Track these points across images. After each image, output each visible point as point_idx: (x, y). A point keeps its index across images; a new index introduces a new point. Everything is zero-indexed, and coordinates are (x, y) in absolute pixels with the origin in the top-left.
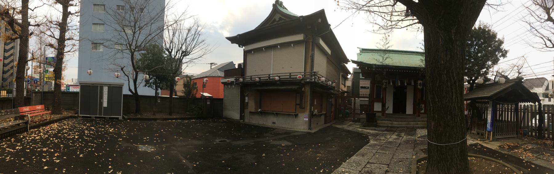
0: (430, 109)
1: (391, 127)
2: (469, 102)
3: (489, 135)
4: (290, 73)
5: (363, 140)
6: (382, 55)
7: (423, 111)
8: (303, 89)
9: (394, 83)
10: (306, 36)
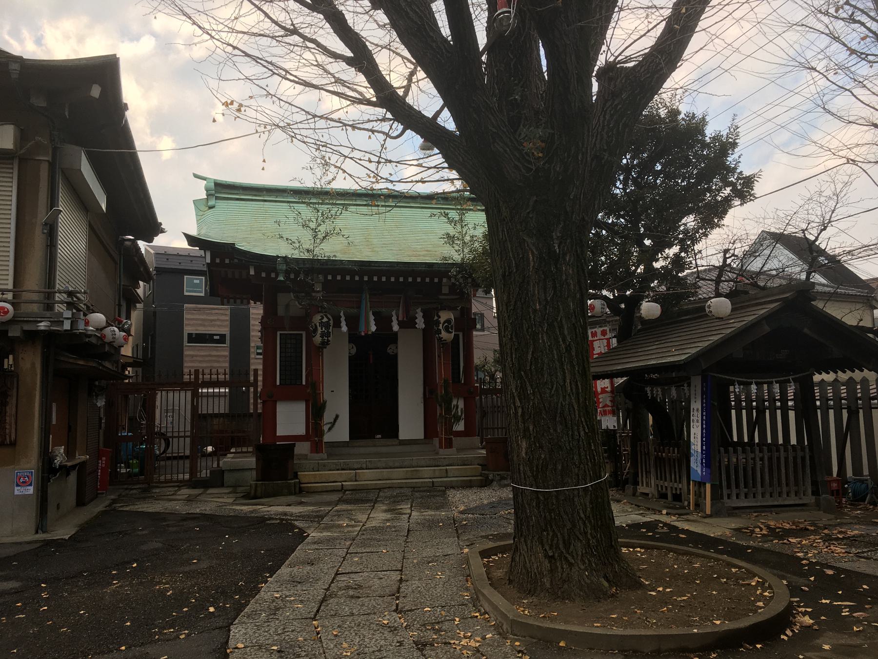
0: (516, 413)
1: (354, 490)
2: (620, 381)
3: (700, 495)
5: (284, 539)
6: (306, 212)
7: (460, 427)
9: (353, 322)
10: (22, 137)
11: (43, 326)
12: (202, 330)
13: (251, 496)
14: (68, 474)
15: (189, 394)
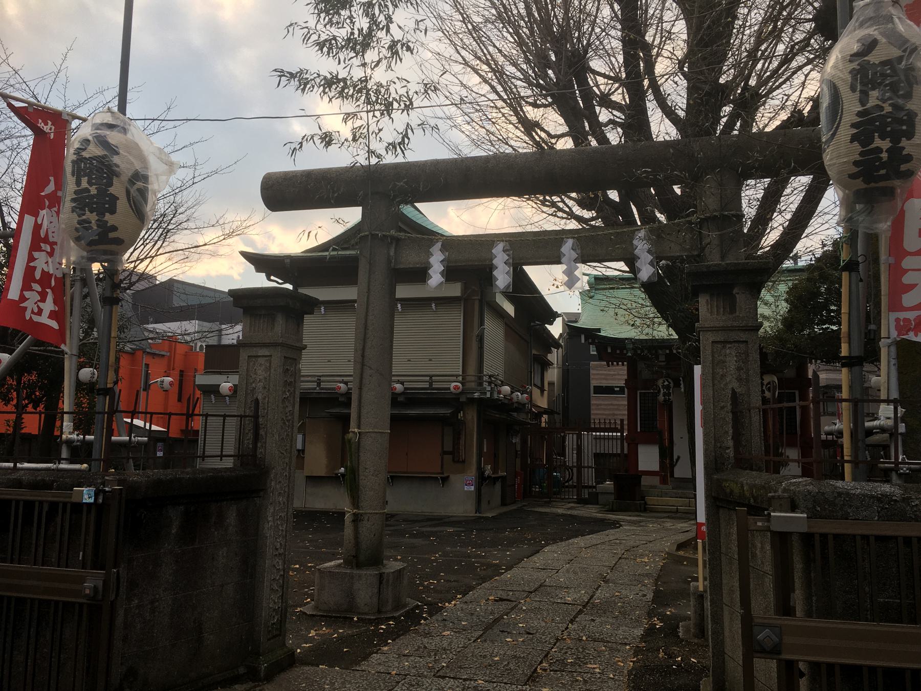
4: (431, 377)
8: (461, 415)
10: (465, 289)
11: (476, 395)
12: (604, 383)
13: (612, 511)
14: (495, 483)
15: (575, 436)
